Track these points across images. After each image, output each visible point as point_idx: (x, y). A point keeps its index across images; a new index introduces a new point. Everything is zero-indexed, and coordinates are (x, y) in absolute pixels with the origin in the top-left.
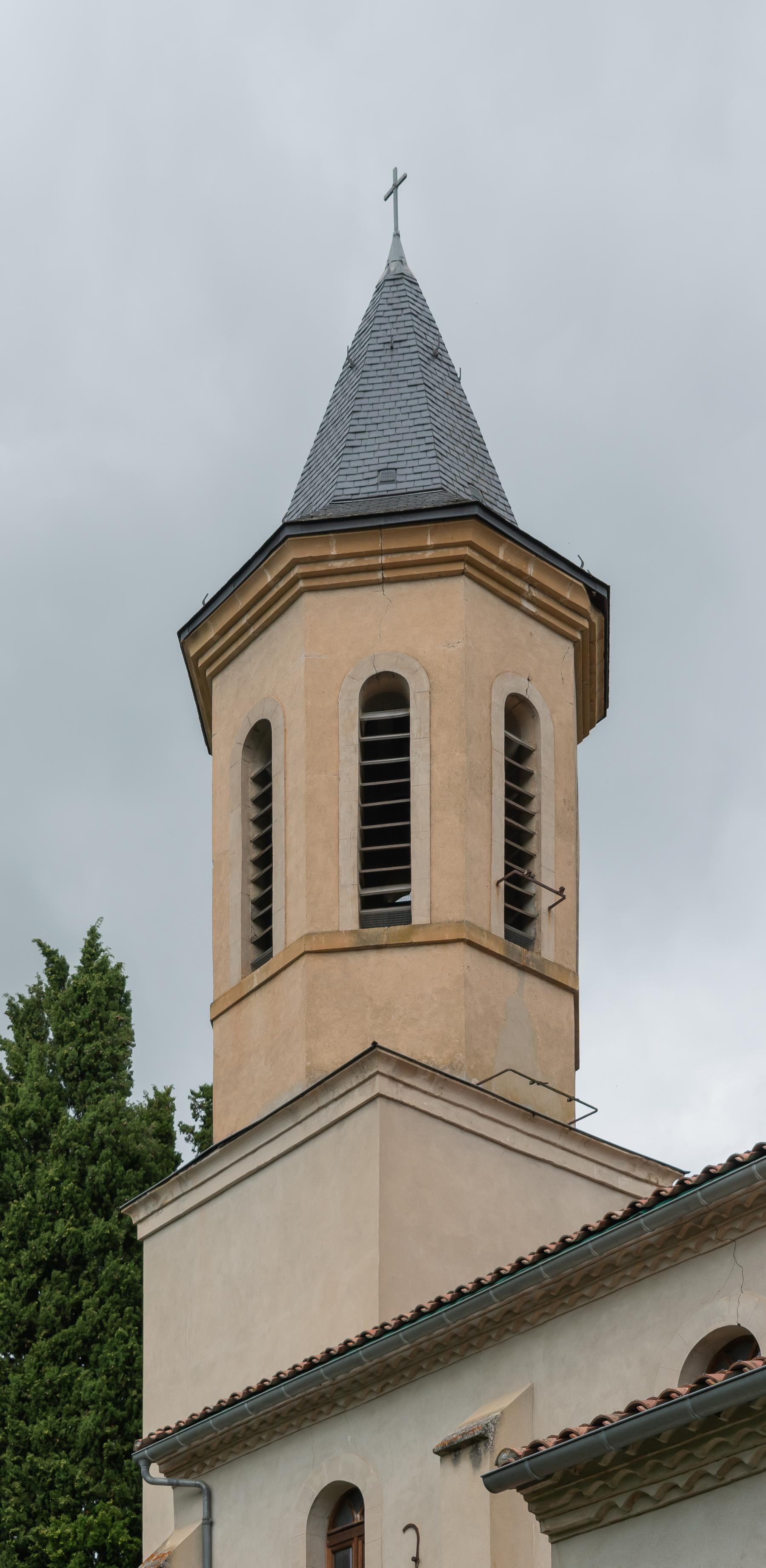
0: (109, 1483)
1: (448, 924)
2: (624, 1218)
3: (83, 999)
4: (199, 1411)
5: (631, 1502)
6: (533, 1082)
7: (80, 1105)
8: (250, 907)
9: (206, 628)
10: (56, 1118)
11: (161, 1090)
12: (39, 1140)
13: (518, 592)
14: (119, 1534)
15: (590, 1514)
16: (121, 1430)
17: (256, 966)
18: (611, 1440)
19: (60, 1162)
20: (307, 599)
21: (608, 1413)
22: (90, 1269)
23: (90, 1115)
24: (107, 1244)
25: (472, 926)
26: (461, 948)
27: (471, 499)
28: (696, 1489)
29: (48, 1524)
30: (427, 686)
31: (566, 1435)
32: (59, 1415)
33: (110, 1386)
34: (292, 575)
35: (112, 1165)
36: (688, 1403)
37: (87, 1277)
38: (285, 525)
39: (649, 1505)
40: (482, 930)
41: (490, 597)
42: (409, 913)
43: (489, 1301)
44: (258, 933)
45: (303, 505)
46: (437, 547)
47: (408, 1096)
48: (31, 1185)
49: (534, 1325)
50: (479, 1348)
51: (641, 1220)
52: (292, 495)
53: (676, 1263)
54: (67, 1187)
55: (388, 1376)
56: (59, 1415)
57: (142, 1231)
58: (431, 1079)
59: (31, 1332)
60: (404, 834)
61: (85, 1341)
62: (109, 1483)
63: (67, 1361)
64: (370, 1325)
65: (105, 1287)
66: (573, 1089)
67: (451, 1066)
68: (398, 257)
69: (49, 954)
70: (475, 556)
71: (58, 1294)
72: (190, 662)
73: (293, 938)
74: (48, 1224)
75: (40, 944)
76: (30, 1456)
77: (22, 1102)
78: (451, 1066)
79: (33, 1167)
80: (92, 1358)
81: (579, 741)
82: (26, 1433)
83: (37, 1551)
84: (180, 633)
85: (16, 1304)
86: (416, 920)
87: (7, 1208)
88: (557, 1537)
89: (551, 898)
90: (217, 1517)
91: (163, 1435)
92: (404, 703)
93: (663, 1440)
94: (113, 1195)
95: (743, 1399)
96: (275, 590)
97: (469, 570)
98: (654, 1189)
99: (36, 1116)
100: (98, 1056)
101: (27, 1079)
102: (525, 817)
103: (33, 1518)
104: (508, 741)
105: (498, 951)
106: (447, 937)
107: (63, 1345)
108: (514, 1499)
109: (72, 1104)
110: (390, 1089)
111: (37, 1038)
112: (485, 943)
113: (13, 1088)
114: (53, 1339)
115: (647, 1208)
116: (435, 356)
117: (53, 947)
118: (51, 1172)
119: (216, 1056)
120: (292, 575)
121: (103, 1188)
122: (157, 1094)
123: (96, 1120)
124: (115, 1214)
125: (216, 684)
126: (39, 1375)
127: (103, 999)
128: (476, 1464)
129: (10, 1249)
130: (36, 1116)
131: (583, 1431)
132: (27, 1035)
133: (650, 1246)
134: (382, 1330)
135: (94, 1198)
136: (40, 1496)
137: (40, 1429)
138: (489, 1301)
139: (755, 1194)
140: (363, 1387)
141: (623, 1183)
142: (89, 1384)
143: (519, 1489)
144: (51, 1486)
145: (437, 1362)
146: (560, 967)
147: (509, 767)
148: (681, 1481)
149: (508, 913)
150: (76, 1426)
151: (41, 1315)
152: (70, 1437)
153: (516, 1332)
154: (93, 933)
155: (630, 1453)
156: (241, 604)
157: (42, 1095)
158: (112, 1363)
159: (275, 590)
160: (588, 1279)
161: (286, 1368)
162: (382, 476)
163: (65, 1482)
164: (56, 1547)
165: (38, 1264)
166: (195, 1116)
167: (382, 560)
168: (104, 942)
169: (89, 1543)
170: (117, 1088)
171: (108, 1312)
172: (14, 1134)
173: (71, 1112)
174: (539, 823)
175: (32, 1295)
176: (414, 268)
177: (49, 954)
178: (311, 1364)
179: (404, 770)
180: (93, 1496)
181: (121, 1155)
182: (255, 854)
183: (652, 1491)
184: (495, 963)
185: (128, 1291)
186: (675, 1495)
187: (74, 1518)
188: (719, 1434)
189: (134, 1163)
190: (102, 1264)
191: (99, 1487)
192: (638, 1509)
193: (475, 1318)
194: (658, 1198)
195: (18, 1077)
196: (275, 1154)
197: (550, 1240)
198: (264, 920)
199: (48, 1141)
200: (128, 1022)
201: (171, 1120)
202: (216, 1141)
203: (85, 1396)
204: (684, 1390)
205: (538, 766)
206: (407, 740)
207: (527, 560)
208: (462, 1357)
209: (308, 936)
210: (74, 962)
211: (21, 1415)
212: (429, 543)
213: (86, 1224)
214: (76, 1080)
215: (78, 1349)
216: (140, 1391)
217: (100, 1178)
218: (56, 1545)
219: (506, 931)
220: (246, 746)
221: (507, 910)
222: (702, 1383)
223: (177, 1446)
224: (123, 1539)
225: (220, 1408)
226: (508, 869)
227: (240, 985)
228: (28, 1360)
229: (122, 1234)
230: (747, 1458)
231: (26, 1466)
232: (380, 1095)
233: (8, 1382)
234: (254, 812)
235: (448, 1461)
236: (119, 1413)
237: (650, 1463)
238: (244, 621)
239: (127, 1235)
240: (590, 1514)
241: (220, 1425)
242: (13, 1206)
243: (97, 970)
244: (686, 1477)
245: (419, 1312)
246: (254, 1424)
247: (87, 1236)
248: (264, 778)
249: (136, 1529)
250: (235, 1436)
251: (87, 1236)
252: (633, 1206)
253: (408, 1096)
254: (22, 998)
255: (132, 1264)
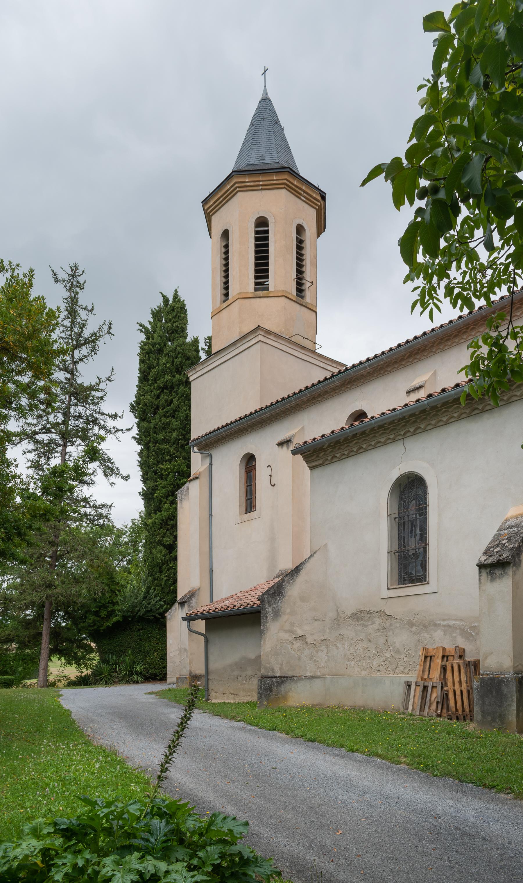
0: (181, 453)
1: (280, 291)
2: (330, 378)
3: (173, 310)
4: (208, 432)
5: (332, 458)
6: (304, 338)
7: (172, 341)
8: (222, 284)
9: (210, 201)
10: (165, 345)
11: (195, 337)
12: (160, 351)
13: (300, 194)
14: (184, 468)
15: (321, 462)
16: (184, 437)
17: (224, 301)
18: (327, 441)
19: (166, 358)
20: (239, 194)
21: (326, 433)
22: (175, 390)
23: (175, 344)
24: (180, 382)
25: (287, 292)
26: (284, 298)
27: (287, 166)
28: (350, 455)
29: (163, 465)
30: (274, 221)
31: (314, 439)
32: (166, 433)
33: (181, 424)
34: (235, 186)
35: (182, 359)
36: (348, 431)
37: (174, 392)
38: (233, 172)
39: (337, 460)
40: (289, 293)
41: (292, 195)
42: (269, 287)
43: (292, 401)
44: (225, 292)
45: (238, 165)
46: (277, 180)
47: (268, 341)
48: (158, 364)
49: (304, 408)
50: (289, 415)
51: (335, 379)
52: (235, 162)
53: (344, 391)
54: (168, 365)
55: (263, 422)
56: (166, 433)
57: (191, 379)
58: (275, 336)
59: (158, 408)
60: (267, 264)
61: (174, 411)
62: (181, 453)
63: (168, 417)
64: (258, 408)
65: (180, 395)
66: (315, 340)
67: (280, 333)
68: (265, 93)
69: (164, 296)
70: (288, 183)
71: (166, 397)
72: (205, 211)
73: (235, 294)
74: (162, 376)
75: (161, 293)
76: (157, 444)
77: (155, 340)
78: (280, 333)
79: (158, 359)
80: (176, 416)
81: (317, 238)
82: (156, 438)
83: (160, 472)
84: (202, 202)
85: (154, 400)
86: (270, 289)
87: (151, 371)
88: (312, 468)
89: (309, 284)
90: (213, 463)
91: (198, 439)
92: (267, 226)
93: (341, 441)
94: (182, 368)
95: (363, 430)
96: (230, 191)
97: (286, 187)
98: (338, 370)
99: (159, 344)
100: (178, 327)
101: (156, 333)
102: (302, 260)
103: (158, 463)
104: (297, 238)
105: (294, 299)
106: (279, 295)
107: (167, 412)
108: (299, 457)
109: (170, 341)
110: (263, 339)
111: (160, 321)
112: (290, 297)
113: (153, 336)
114: (164, 410)
115: (336, 375)
116: (276, 123)
117: (165, 295)
118: (164, 361)
119: (213, 328)
120: (235, 186)
121: (179, 366)
122: (194, 338)
123: (177, 346)
124: (183, 374)
125: (213, 218)
126: (160, 421)
127: (179, 310)
128: (288, 448)
129: (152, 383)
130: (159, 344)
131: (319, 438)
132: (157, 320)
133: (337, 386)
134: (261, 409)
135: (176, 369)
136: (160, 456)
137: (160, 436)
138: (292, 401)
139: (367, 372)
140: (256, 425)
141: (329, 368)
142: (175, 423)
143: (301, 454)
144: (164, 453)
145: (277, 419)
146: (312, 305)
147: (297, 246)
148: (346, 453)
149: (297, 288)
150: (171, 436)
151: (161, 403)
152: (169, 439)
153: (299, 410)
154: (176, 291)
155: (332, 444)
156: (220, 194)
157: (161, 338)
158: (182, 418)
159: (230, 191)
160: (320, 395)
161: (233, 420)
162: (261, 158)
163: (168, 452)
164: (165, 471)
165: (160, 388)
166: (206, 345)
167: (261, 183)
168: (179, 293)
169: (175, 470)
170: (183, 337)
171: (180, 402)
172: (153, 349)
173: (170, 343)
174: (306, 262)
175: (158, 397)
176: (270, 96)
177: (164, 296)
178: (241, 419)
179: (267, 245)
180: (176, 456)
181: (184, 356)
182: (224, 268)
183: (338, 455)
184: (293, 303)
185: (186, 396)
186: (344, 457)
187: (171, 463)
188: (357, 440)
189: (188, 359)
190: (179, 389)
191: (178, 454)
192: (334, 460)
193: (288, 406)
194: (340, 372)
195: (154, 332)
196: (230, 357)
197: (309, 384)
198: (227, 288)
199: (163, 352)
200: (186, 317)
201: (198, 346)
202: (213, 353)
203: (174, 427)
204: (347, 427)
205: (306, 246)
206: (268, 237)
207: (303, 184)
208: (284, 417)
209: (239, 293)
210: (171, 299)
211: (155, 433)
212: (275, 178)
213: (174, 376)
214: (171, 334)
215: (172, 413)
216: (190, 426)
217: (178, 363)
218: (165, 471)
219: (297, 294)
220: (222, 236)
221: (297, 287)
222: (352, 425)
223: (202, 442)
224: (185, 469)
225: (214, 431)
226: (297, 275)
227: (220, 307)
228: (157, 416)
229: (184, 380)
230: (364, 446)
231: (156, 448)
232: (260, 341)
233: (151, 423)
234: (224, 256)
235: (280, 447)
236: (184, 432)
237: (338, 447)
238: (221, 199)
239: (186, 380)
240: (321, 462)
241: (214, 436)
242: (152, 370)
243: (177, 301)
244: (347, 451)
245: (272, 404)
246: (224, 436)
247: (174, 380)
248: (227, 246)
249: (189, 466)
250: (219, 439)
251: (174, 380)
252: (339, 371)
253: (268, 341)
254: (155, 309)
255: (187, 388)
